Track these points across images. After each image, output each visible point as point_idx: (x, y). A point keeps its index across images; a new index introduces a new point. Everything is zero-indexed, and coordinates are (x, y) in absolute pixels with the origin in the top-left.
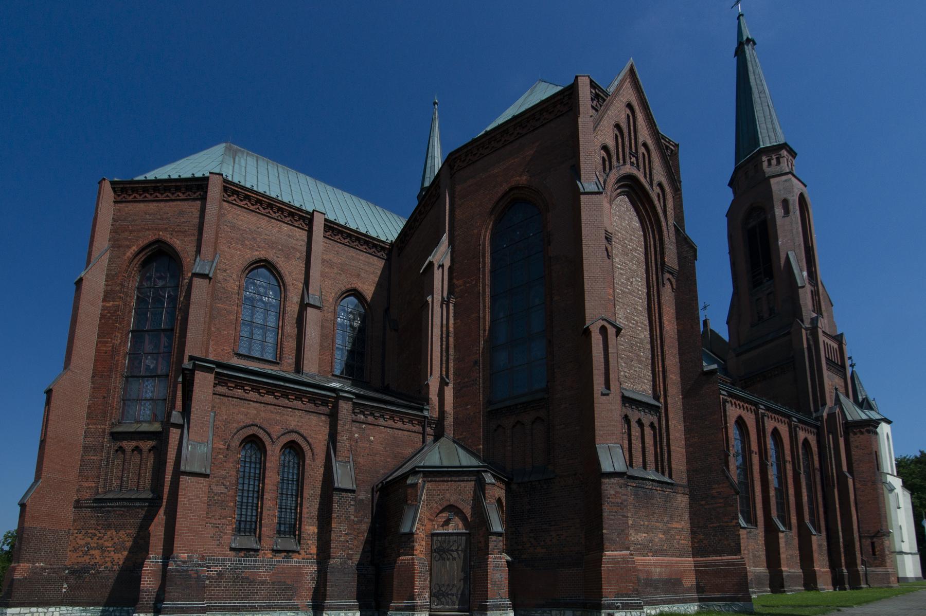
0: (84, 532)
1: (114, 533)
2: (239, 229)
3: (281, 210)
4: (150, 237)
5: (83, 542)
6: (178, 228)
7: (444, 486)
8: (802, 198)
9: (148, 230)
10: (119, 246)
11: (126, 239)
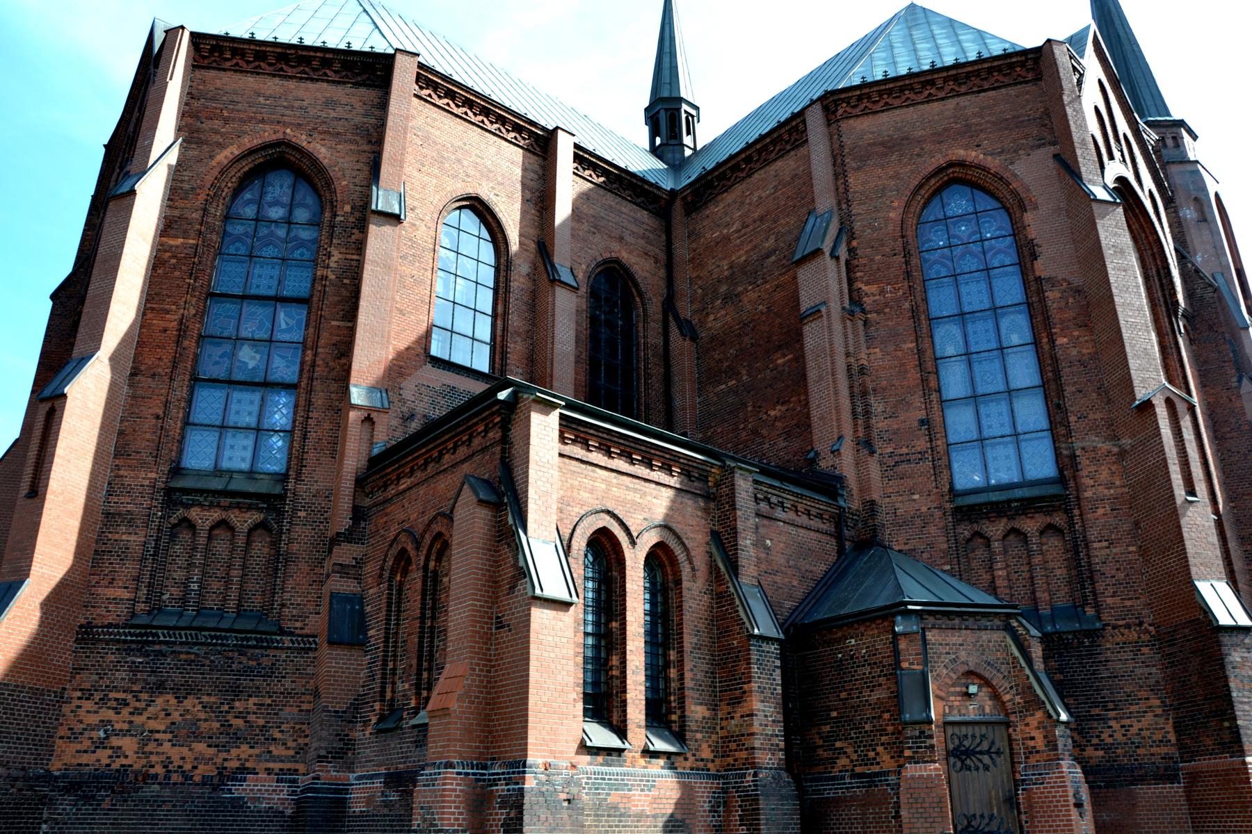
0: (97, 697)
1: (173, 701)
2: (435, 142)
3: (502, 120)
4: (268, 134)
5: (93, 719)
6: (324, 127)
7: (955, 638)
8: (1217, 195)
9: (263, 121)
10: (200, 142)
11: (217, 132)
